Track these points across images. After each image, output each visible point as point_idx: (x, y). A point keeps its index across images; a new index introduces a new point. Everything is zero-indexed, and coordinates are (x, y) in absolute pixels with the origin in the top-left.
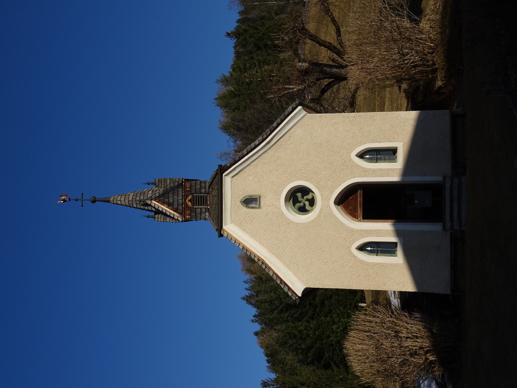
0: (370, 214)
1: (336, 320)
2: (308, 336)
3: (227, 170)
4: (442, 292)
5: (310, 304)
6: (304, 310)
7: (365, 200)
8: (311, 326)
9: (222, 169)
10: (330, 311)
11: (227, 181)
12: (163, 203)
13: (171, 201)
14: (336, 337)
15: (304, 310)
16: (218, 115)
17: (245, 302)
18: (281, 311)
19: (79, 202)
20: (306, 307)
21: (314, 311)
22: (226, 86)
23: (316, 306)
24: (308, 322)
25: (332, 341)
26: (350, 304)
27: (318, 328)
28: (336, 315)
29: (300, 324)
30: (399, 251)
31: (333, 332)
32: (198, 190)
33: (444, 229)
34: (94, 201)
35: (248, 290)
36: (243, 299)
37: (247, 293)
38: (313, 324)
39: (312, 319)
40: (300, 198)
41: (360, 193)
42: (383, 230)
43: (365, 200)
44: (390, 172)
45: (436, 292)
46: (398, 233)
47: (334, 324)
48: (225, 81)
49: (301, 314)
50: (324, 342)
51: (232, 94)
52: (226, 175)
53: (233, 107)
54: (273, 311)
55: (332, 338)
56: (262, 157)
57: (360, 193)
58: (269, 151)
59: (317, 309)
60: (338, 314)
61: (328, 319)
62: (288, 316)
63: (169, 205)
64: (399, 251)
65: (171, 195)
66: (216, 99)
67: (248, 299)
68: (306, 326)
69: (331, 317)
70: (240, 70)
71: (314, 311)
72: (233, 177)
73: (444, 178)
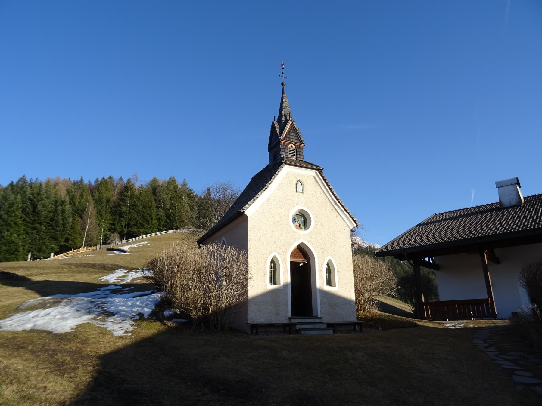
0: (294, 266)
1: (21, 237)
2: (10, 217)
3: (320, 173)
4: (249, 317)
5: (35, 220)
6: (31, 216)
7: (302, 265)
8: (18, 220)
9: (320, 170)
10: (27, 233)
11: (312, 173)
12: (289, 129)
13: (291, 134)
14: (7, 236)
15: (31, 216)
16: (163, 178)
17: (21, 177)
18: (31, 200)
19: (281, 75)
20: (33, 217)
21: (29, 223)
22: (182, 185)
23: (32, 224)
24: (21, 217)
25: (4, 233)
26: (32, 247)
27: (15, 224)
28: (25, 237)
29: (20, 212)
30: (273, 287)
31: (11, 234)
32: (298, 153)
33: (290, 318)
34: (283, 84)
35: (31, 180)
36: (24, 176)
37: (28, 179)
38: (20, 221)
39: (24, 221)
40: (303, 219)
41: (305, 261)
42: (285, 277)
43: (302, 265)
44: (320, 281)
45: (249, 312)
46: (285, 286)
47: (18, 235)
48: (184, 185)
49: (28, 213)
50: (4, 227)
51: (176, 187)
52: (316, 173)
53: (168, 187)
54: (32, 194)
55: (6, 233)
56: (326, 198)
57: (305, 261)
58: (329, 203)
59: (30, 225)
60: (25, 239)
61: (22, 232)
62: (27, 204)
63: (289, 132)
64: (273, 287)
65: (294, 134)
66: (174, 178)
67: (23, 179)
68: (18, 216)
69: (23, 234)
70: (190, 194)
71: (29, 223)
72: (314, 177)
73: (320, 318)
